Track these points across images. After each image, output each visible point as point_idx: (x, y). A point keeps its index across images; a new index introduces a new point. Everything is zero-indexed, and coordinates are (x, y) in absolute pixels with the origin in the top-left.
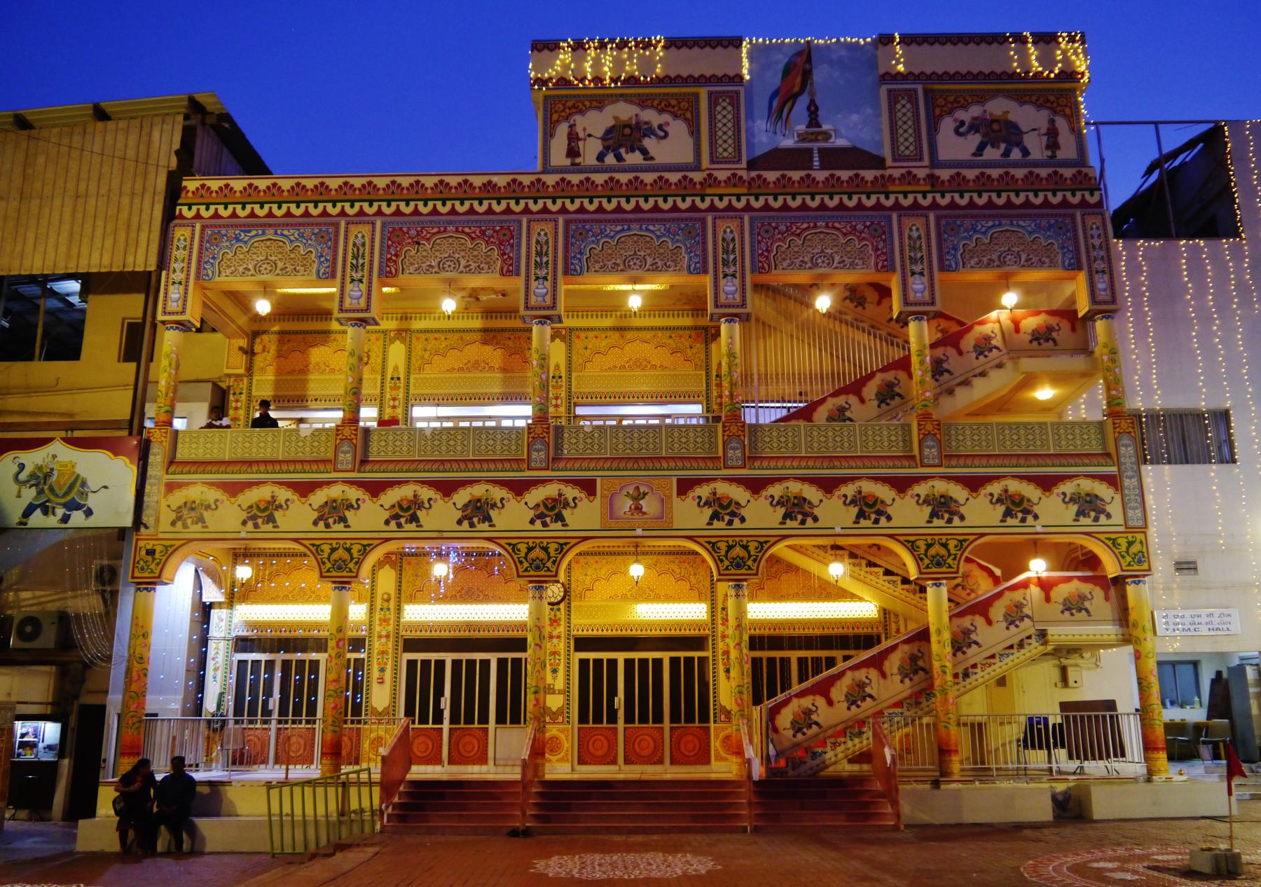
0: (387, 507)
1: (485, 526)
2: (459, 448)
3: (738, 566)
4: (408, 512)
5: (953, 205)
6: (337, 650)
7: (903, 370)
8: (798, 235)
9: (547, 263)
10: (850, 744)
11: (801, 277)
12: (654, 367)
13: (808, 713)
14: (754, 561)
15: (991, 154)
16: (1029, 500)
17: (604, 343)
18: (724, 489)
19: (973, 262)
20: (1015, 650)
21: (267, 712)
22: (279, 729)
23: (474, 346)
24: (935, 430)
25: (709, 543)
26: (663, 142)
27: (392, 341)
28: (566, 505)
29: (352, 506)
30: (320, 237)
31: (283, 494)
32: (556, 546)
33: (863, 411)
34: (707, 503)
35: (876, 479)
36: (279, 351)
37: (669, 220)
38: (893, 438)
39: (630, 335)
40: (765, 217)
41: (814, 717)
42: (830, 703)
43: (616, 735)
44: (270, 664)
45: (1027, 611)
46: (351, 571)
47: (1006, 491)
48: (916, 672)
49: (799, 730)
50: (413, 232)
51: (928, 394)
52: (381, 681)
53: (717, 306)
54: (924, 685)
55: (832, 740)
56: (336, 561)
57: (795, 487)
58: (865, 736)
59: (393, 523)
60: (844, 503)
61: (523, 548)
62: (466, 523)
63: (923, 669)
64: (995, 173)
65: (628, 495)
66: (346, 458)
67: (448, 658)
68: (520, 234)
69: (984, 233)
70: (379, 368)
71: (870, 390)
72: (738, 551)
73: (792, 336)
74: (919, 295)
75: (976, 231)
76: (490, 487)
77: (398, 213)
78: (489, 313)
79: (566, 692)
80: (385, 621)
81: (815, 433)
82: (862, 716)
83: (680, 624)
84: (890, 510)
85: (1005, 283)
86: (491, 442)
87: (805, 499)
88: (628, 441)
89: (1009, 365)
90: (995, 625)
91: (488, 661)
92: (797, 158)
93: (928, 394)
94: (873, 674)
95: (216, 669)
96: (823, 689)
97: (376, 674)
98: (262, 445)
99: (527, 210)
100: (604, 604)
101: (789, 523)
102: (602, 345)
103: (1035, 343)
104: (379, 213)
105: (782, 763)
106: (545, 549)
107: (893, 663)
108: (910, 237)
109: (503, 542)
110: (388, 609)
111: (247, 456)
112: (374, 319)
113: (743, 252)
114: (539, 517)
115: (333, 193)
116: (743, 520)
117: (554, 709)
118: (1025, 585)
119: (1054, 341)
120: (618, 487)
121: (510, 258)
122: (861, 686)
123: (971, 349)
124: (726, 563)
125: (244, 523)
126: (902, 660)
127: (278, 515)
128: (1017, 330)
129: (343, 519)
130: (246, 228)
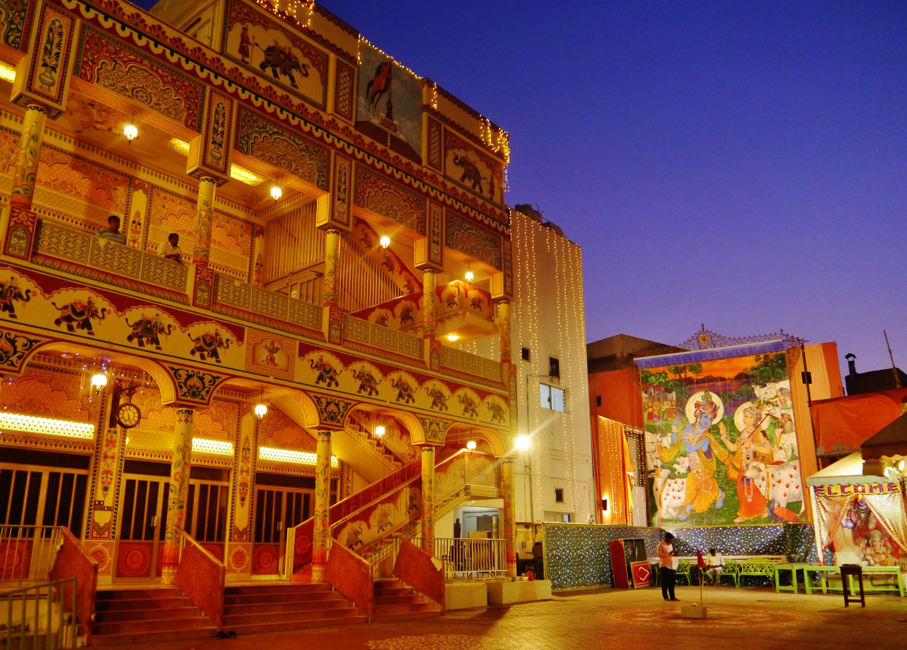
0: (60, 306)
1: (152, 347)
5: (373, 166)
10: (374, 557)
15: (468, 183)
23: (64, 167)
26: (304, 78)
29: (21, 296)
41: (360, 537)
42: (369, 527)
62: (135, 340)
64: (280, 92)
65: (266, 347)
76: (160, 312)
83: (212, 458)
86: (159, 271)
92: (377, 133)
100: (155, 432)
113: (230, 128)
117: (102, 525)
120: (260, 339)
128: (466, 296)
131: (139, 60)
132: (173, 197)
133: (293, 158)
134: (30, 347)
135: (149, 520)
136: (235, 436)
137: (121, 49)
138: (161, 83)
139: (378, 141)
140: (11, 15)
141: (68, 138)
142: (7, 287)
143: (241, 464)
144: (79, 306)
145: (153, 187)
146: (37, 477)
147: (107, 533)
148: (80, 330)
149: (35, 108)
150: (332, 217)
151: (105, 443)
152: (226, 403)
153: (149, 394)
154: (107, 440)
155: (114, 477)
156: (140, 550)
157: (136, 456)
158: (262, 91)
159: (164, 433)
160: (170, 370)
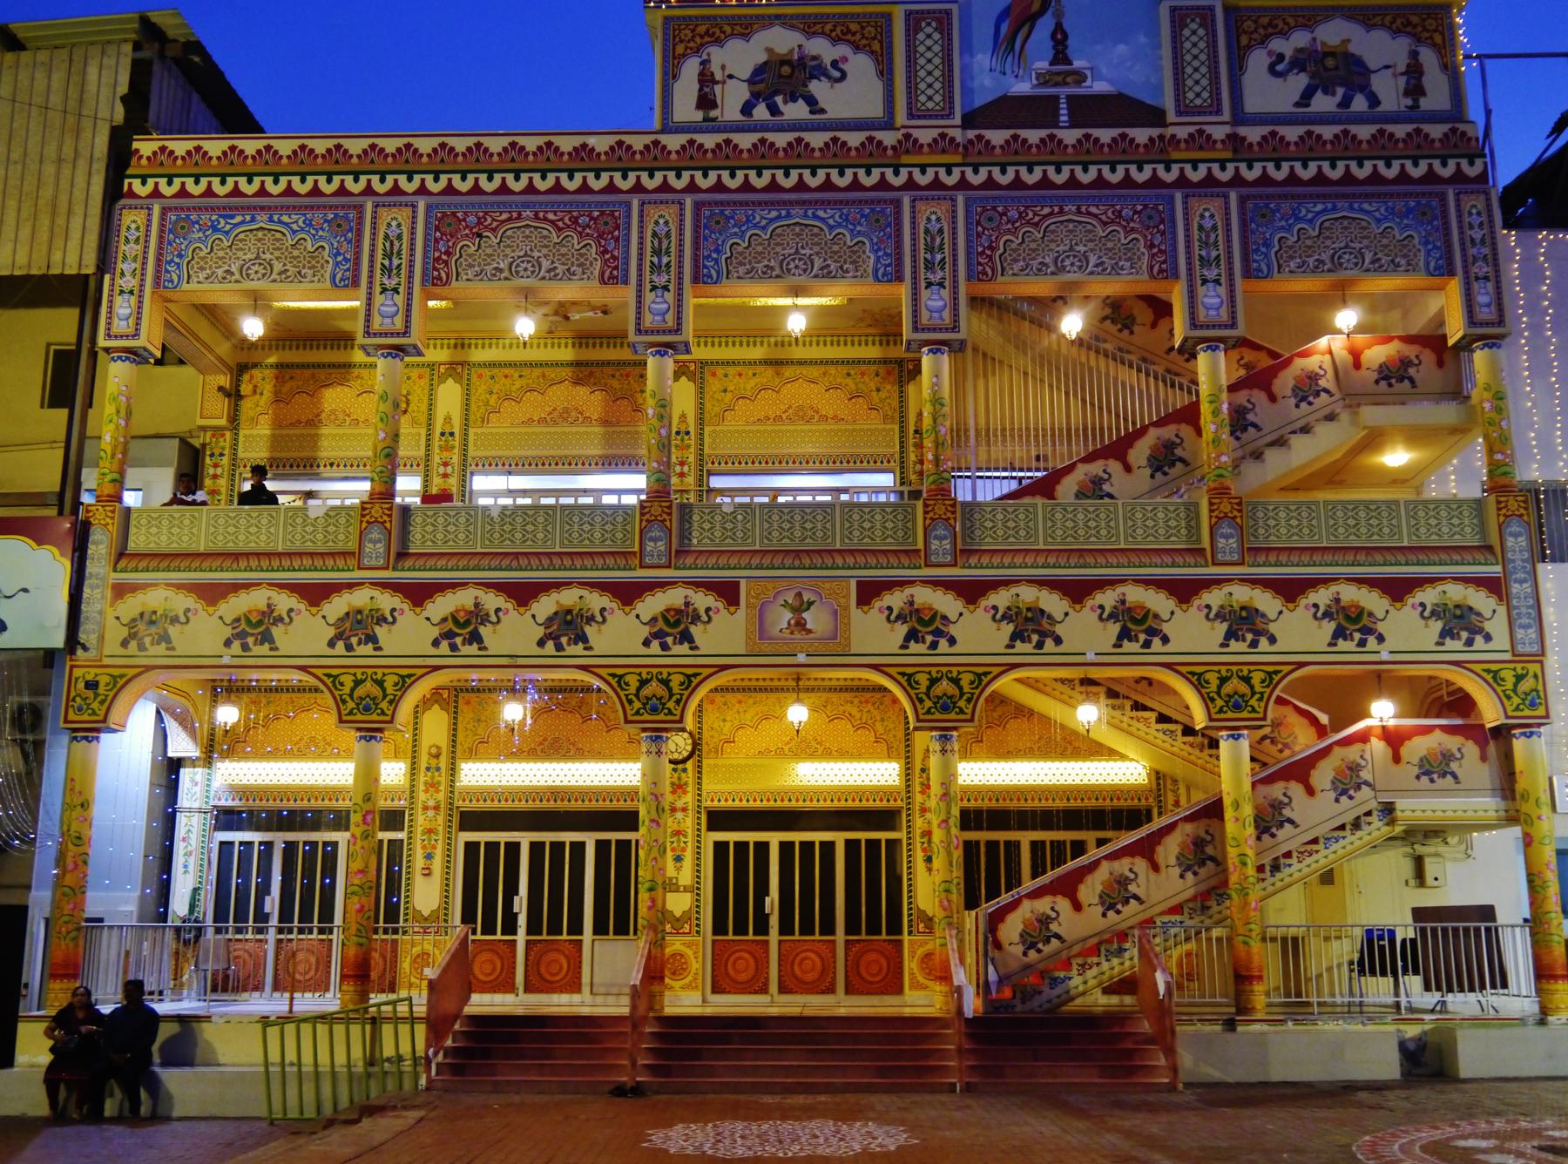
1: (578, 649)
3: (945, 709)
4: (466, 629)
5: (1265, 179)
7: (1188, 422)
8: (1036, 225)
9: (668, 265)
10: (1105, 966)
12: (824, 418)
13: (1044, 921)
16: (1371, 614)
17: (752, 383)
18: (925, 596)
20: (1347, 833)
21: (262, 917)
22: (279, 941)
24: (1234, 510)
27: (442, 380)
28: (696, 618)
29: (385, 620)
30: (336, 225)
31: (284, 602)
33: (1129, 483)
35: (1147, 582)
36: (276, 393)
38: (1173, 523)
39: (788, 372)
40: (987, 199)
41: (1054, 927)
42: (1077, 906)
43: (767, 951)
44: (268, 846)
45: (1365, 775)
46: (383, 713)
47: (1337, 601)
48: (1202, 863)
49: (1033, 946)
50: (472, 219)
52: (427, 872)
53: (916, 329)
54: (1213, 882)
55: (1080, 960)
56: (361, 699)
57: (1028, 594)
58: (1127, 955)
59: (445, 644)
60: (1100, 618)
61: (633, 681)
62: (550, 645)
63: (1212, 859)
64: (1327, 132)
65: (786, 604)
66: (375, 550)
67: (525, 839)
69: (1311, 221)
71: (1140, 453)
72: (945, 687)
73: (1026, 374)
75: (1298, 219)
76: (584, 592)
80: (432, 785)
81: (1058, 516)
82: (1124, 926)
83: (860, 793)
85: (1340, 295)
87: (1042, 612)
88: (786, 526)
89: (1344, 417)
90: (1319, 795)
91: (583, 844)
93: (1224, 459)
95: (188, 854)
96: (1068, 887)
97: (419, 862)
98: (253, 530)
99: (638, 188)
100: (750, 762)
101: (1020, 646)
104: (422, 190)
105: (1007, 993)
106: (666, 683)
107: (1169, 850)
110: (438, 769)
111: (231, 547)
112: (415, 347)
114: (656, 635)
118: (1363, 737)
120: (771, 594)
121: (615, 258)
122: (1123, 882)
123: (1289, 393)
125: (228, 643)
126: (1183, 846)
128: (1357, 365)
129: (372, 639)
130: (227, 212)
132: (739, 369)
135: (759, 904)
136: (902, 746)
146: (578, 848)
153: (734, 701)
155: (689, 839)
157: (723, 803)
158: (817, 154)
159: (766, 762)
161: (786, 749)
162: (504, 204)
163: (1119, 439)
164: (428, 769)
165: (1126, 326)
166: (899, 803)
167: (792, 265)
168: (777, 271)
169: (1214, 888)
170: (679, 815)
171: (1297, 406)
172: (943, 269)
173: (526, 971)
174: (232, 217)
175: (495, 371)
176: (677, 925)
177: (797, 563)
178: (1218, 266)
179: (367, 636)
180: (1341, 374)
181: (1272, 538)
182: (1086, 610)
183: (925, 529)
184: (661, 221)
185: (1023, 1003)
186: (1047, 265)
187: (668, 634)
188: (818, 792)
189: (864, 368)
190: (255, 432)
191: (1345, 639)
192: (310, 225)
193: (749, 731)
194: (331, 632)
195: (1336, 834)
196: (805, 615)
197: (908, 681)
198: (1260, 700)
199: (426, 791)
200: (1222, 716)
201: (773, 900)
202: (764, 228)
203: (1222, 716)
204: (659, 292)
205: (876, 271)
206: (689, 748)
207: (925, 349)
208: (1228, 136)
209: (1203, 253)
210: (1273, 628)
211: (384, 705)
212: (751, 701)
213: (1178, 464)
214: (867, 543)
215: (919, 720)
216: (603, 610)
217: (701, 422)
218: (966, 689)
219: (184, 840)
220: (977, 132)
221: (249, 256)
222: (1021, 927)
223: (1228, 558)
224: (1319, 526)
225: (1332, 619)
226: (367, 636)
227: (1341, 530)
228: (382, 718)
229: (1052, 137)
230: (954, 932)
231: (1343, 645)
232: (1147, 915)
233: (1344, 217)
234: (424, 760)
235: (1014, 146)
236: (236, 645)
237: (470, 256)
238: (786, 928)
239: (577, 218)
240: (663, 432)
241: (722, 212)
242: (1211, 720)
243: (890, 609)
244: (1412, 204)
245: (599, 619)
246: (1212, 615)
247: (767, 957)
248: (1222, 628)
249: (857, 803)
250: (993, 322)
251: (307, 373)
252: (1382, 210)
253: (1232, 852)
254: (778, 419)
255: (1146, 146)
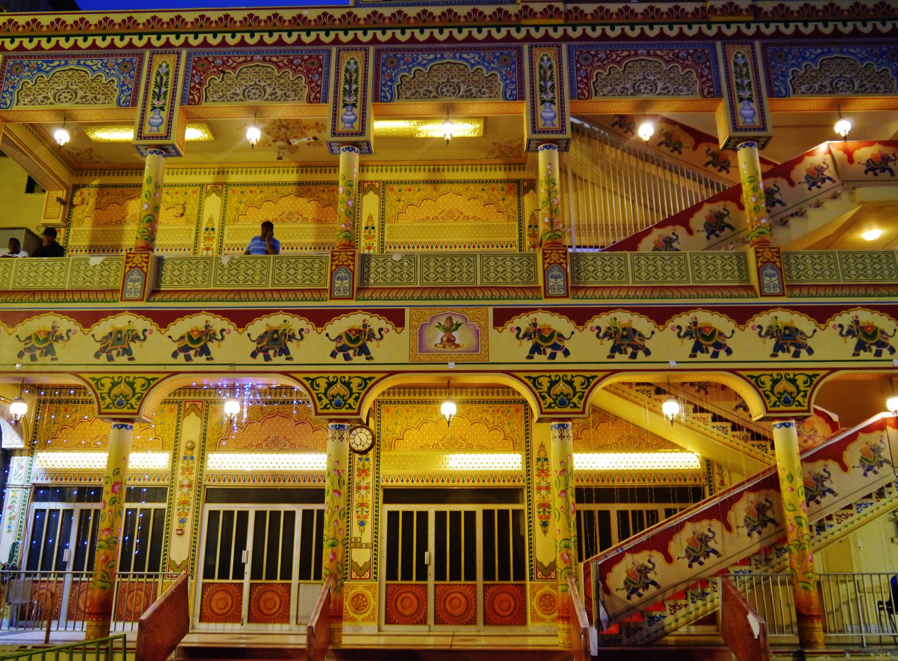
1: (282, 359)
2: (258, 278)
3: (563, 404)
4: (199, 344)
5: (778, 34)
6: (111, 495)
7: (732, 200)
8: (619, 63)
9: (356, 90)
10: (692, 607)
11: (619, 106)
12: (467, 218)
13: (643, 571)
14: (580, 398)
16: (883, 332)
17: (418, 195)
18: (545, 320)
19: (803, 88)
20: (874, 500)
21: (61, 565)
22: (74, 582)
23: (289, 198)
24: (775, 259)
25: (529, 378)
27: (208, 194)
28: (371, 336)
29: (138, 337)
30: (123, 67)
31: (65, 325)
32: (359, 381)
33: (692, 243)
34: (527, 335)
35: (712, 309)
36: (97, 203)
37: (484, 49)
38: (728, 267)
39: (443, 188)
40: (583, 46)
41: (651, 576)
42: (669, 559)
43: (426, 592)
44: (68, 513)
45: (885, 455)
46: (132, 407)
47: (857, 322)
48: (764, 525)
49: (634, 591)
50: (219, 62)
51: (763, 221)
52: (181, 532)
53: (534, 131)
54: (774, 539)
55: (672, 603)
56: (117, 396)
57: (623, 318)
58: (708, 598)
59: (181, 356)
60: (679, 335)
61: (323, 383)
62: (261, 356)
63: (772, 521)
66: (134, 286)
67: (252, 509)
68: (329, 63)
69: (814, 60)
70: (194, 219)
71: (698, 221)
72: (562, 387)
73: (604, 188)
74: (748, 120)
75: (805, 59)
76: (288, 317)
77: (205, 44)
78: (304, 167)
79: (374, 546)
80: (187, 470)
81: (643, 262)
82: (705, 575)
83: (494, 476)
84: (729, 343)
85: (838, 109)
86: (292, 271)
87: (634, 331)
88: (440, 270)
89: (845, 196)
90: (851, 471)
91: (293, 513)
93: (763, 221)
94: (717, 526)
95: (12, 518)
96: (660, 543)
97: (175, 525)
98: (49, 274)
99: (337, 41)
100: (415, 453)
101: (618, 357)
102: (415, 198)
103: (870, 173)
104: (186, 44)
105: (614, 629)
106: (347, 384)
107: (739, 513)
108: (736, 64)
109: (300, 376)
110: (192, 458)
111: (31, 286)
112: (174, 147)
114: (340, 349)
115: (141, 26)
116: (567, 353)
118: (881, 426)
119: (891, 171)
120: (428, 318)
121: (318, 86)
122: (703, 540)
123: (803, 180)
124: (549, 400)
125: (21, 355)
126: (748, 510)
127: (57, 346)
128: (851, 160)
129: (128, 352)
130: (49, 58)
131: (826, 50)
132: (409, 186)
133: (854, 74)
134: (811, 383)
135: (421, 557)
136: (523, 443)
137: (229, 58)
138: (858, 62)
139: (480, 3)
140: (122, 79)
141: (290, 169)
142: (124, 332)
143: (536, 480)
144: (196, 333)
145: (385, 183)
146: (290, 515)
147: (553, 574)
148: (357, 357)
149: (746, 145)
150: (735, 127)
151: (356, 473)
152: (505, 406)
153: (403, 410)
154: (359, 469)
155: (370, 509)
156: (413, 594)
157: (394, 483)
159: (425, 453)
160: (305, 381)
161: (441, 444)
162: (242, 52)
163: (687, 209)
164: (185, 458)
165: (675, 149)
166: (522, 483)
167: (445, 90)
168: (434, 94)
169: (775, 544)
170: (363, 492)
171: (810, 189)
172: (553, 91)
173: (250, 606)
174: (52, 62)
175: (244, 188)
176: (361, 573)
177: (448, 296)
178: (750, 89)
179: (124, 349)
180: (839, 167)
181: (803, 278)
182: (668, 329)
183: (544, 271)
184: (352, 62)
185: (628, 637)
186: (627, 89)
187: (350, 348)
188: (462, 476)
189: (493, 185)
190: (80, 228)
191: (865, 351)
192: (106, 66)
193: (414, 431)
194: (98, 346)
195: (865, 501)
196: (453, 334)
197: (534, 383)
198: (804, 396)
199: (183, 474)
200: (776, 409)
201: (430, 554)
202: (424, 66)
203: (776, 409)
204: (349, 108)
205: (505, 93)
206: (370, 442)
207: (541, 146)
208: (750, 6)
209: (739, 81)
210: (810, 342)
211: (133, 401)
212: (415, 410)
213: (726, 229)
214: (500, 282)
215: (542, 413)
216: (301, 330)
217: (382, 220)
218: (578, 389)
219: (10, 508)
220: (574, 5)
221: (62, 87)
222: (625, 575)
223: (772, 291)
224: (837, 270)
225: (854, 336)
226: (124, 349)
227: (853, 272)
228: (131, 411)
229: (627, 8)
230: (574, 580)
231: (863, 355)
232: (724, 566)
233: (837, 57)
234: (182, 452)
235: (600, 14)
236: (27, 356)
237: (216, 85)
238: (440, 575)
239: (292, 61)
240: (350, 203)
241: (395, 56)
242: (768, 412)
243: (519, 329)
244: (885, 49)
245: (298, 337)
246: (763, 333)
247: (426, 597)
248: (771, 343)
249: (491, 484)
250: (584, 146)
251: (119, 190)
252: (864, 53)
253: (789, 515)
254: (435, 218)
255: (692, 13)
